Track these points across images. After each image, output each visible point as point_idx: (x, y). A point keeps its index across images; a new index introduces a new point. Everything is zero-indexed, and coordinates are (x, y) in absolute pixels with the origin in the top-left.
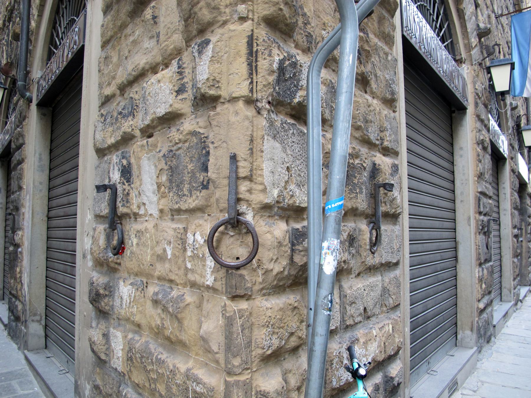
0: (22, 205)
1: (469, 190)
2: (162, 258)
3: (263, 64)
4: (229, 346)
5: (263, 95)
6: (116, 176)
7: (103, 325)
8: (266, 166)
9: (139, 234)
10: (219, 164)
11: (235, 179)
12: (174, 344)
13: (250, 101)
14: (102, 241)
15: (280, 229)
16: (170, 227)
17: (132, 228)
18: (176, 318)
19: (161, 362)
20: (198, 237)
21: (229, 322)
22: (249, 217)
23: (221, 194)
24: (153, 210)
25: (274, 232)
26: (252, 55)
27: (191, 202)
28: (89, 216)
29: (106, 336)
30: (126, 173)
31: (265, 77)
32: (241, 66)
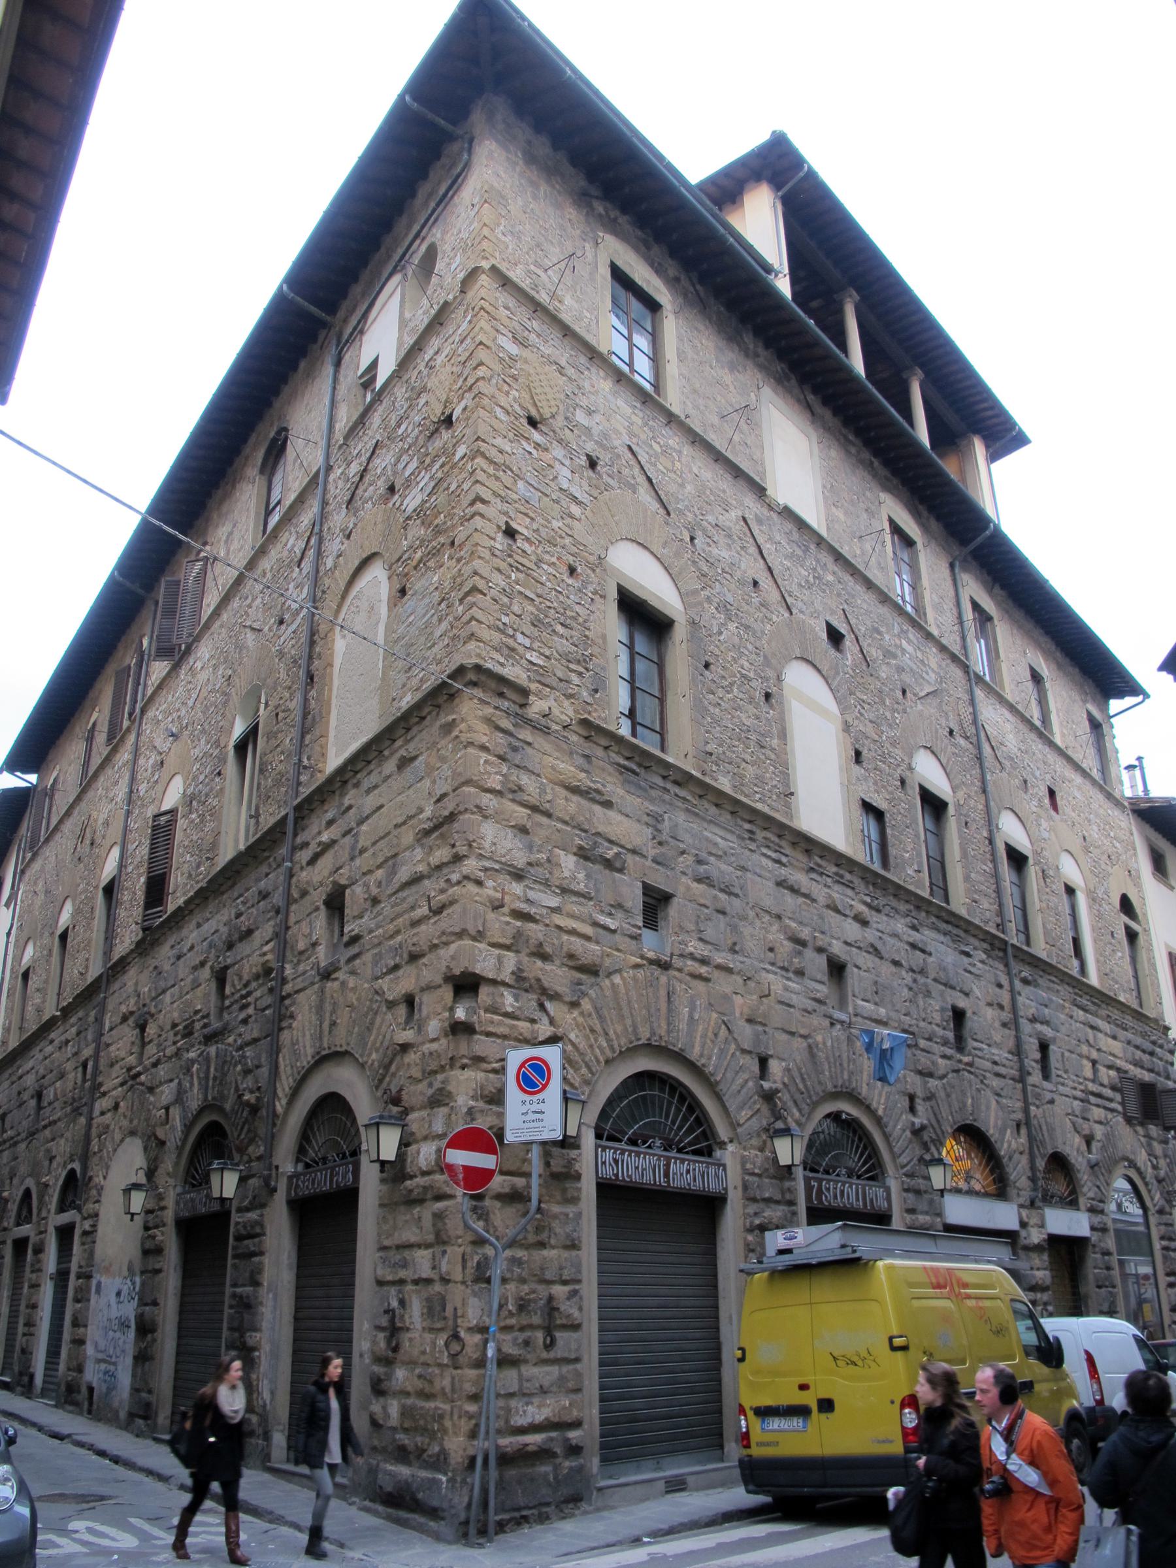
0: (261, 1303)
1: (976, 1262)
2: (424, 1353)
3: (469, 1264)
4: (453, 1390)
5: (469, 1278)
6: (395, 1304)
7: (382, 1399)
8: (470, 1311)
9: (411, 1340)
10: (449, 1312)
11: (456, 1317)
12: (429, 1397)
13: (463, 1283)
14: (383, 1345)
15: (478, 1338)
16: (428, 1336)
17: (405, 1337)
18: (431, 1382)
19: (422, 1408)
20: (441, 1342)
21: (453, 1378)
22: (462, 1334)
23: (451, 1323)
24: (418, 1326)
25: (474, 1339)
26: (464, 1261)
27: (438, 1325)
28: (366, 1326)
29: (384, 1408)
30: (402, 1302)
31: (470, 1271)
32: (459, 1268)
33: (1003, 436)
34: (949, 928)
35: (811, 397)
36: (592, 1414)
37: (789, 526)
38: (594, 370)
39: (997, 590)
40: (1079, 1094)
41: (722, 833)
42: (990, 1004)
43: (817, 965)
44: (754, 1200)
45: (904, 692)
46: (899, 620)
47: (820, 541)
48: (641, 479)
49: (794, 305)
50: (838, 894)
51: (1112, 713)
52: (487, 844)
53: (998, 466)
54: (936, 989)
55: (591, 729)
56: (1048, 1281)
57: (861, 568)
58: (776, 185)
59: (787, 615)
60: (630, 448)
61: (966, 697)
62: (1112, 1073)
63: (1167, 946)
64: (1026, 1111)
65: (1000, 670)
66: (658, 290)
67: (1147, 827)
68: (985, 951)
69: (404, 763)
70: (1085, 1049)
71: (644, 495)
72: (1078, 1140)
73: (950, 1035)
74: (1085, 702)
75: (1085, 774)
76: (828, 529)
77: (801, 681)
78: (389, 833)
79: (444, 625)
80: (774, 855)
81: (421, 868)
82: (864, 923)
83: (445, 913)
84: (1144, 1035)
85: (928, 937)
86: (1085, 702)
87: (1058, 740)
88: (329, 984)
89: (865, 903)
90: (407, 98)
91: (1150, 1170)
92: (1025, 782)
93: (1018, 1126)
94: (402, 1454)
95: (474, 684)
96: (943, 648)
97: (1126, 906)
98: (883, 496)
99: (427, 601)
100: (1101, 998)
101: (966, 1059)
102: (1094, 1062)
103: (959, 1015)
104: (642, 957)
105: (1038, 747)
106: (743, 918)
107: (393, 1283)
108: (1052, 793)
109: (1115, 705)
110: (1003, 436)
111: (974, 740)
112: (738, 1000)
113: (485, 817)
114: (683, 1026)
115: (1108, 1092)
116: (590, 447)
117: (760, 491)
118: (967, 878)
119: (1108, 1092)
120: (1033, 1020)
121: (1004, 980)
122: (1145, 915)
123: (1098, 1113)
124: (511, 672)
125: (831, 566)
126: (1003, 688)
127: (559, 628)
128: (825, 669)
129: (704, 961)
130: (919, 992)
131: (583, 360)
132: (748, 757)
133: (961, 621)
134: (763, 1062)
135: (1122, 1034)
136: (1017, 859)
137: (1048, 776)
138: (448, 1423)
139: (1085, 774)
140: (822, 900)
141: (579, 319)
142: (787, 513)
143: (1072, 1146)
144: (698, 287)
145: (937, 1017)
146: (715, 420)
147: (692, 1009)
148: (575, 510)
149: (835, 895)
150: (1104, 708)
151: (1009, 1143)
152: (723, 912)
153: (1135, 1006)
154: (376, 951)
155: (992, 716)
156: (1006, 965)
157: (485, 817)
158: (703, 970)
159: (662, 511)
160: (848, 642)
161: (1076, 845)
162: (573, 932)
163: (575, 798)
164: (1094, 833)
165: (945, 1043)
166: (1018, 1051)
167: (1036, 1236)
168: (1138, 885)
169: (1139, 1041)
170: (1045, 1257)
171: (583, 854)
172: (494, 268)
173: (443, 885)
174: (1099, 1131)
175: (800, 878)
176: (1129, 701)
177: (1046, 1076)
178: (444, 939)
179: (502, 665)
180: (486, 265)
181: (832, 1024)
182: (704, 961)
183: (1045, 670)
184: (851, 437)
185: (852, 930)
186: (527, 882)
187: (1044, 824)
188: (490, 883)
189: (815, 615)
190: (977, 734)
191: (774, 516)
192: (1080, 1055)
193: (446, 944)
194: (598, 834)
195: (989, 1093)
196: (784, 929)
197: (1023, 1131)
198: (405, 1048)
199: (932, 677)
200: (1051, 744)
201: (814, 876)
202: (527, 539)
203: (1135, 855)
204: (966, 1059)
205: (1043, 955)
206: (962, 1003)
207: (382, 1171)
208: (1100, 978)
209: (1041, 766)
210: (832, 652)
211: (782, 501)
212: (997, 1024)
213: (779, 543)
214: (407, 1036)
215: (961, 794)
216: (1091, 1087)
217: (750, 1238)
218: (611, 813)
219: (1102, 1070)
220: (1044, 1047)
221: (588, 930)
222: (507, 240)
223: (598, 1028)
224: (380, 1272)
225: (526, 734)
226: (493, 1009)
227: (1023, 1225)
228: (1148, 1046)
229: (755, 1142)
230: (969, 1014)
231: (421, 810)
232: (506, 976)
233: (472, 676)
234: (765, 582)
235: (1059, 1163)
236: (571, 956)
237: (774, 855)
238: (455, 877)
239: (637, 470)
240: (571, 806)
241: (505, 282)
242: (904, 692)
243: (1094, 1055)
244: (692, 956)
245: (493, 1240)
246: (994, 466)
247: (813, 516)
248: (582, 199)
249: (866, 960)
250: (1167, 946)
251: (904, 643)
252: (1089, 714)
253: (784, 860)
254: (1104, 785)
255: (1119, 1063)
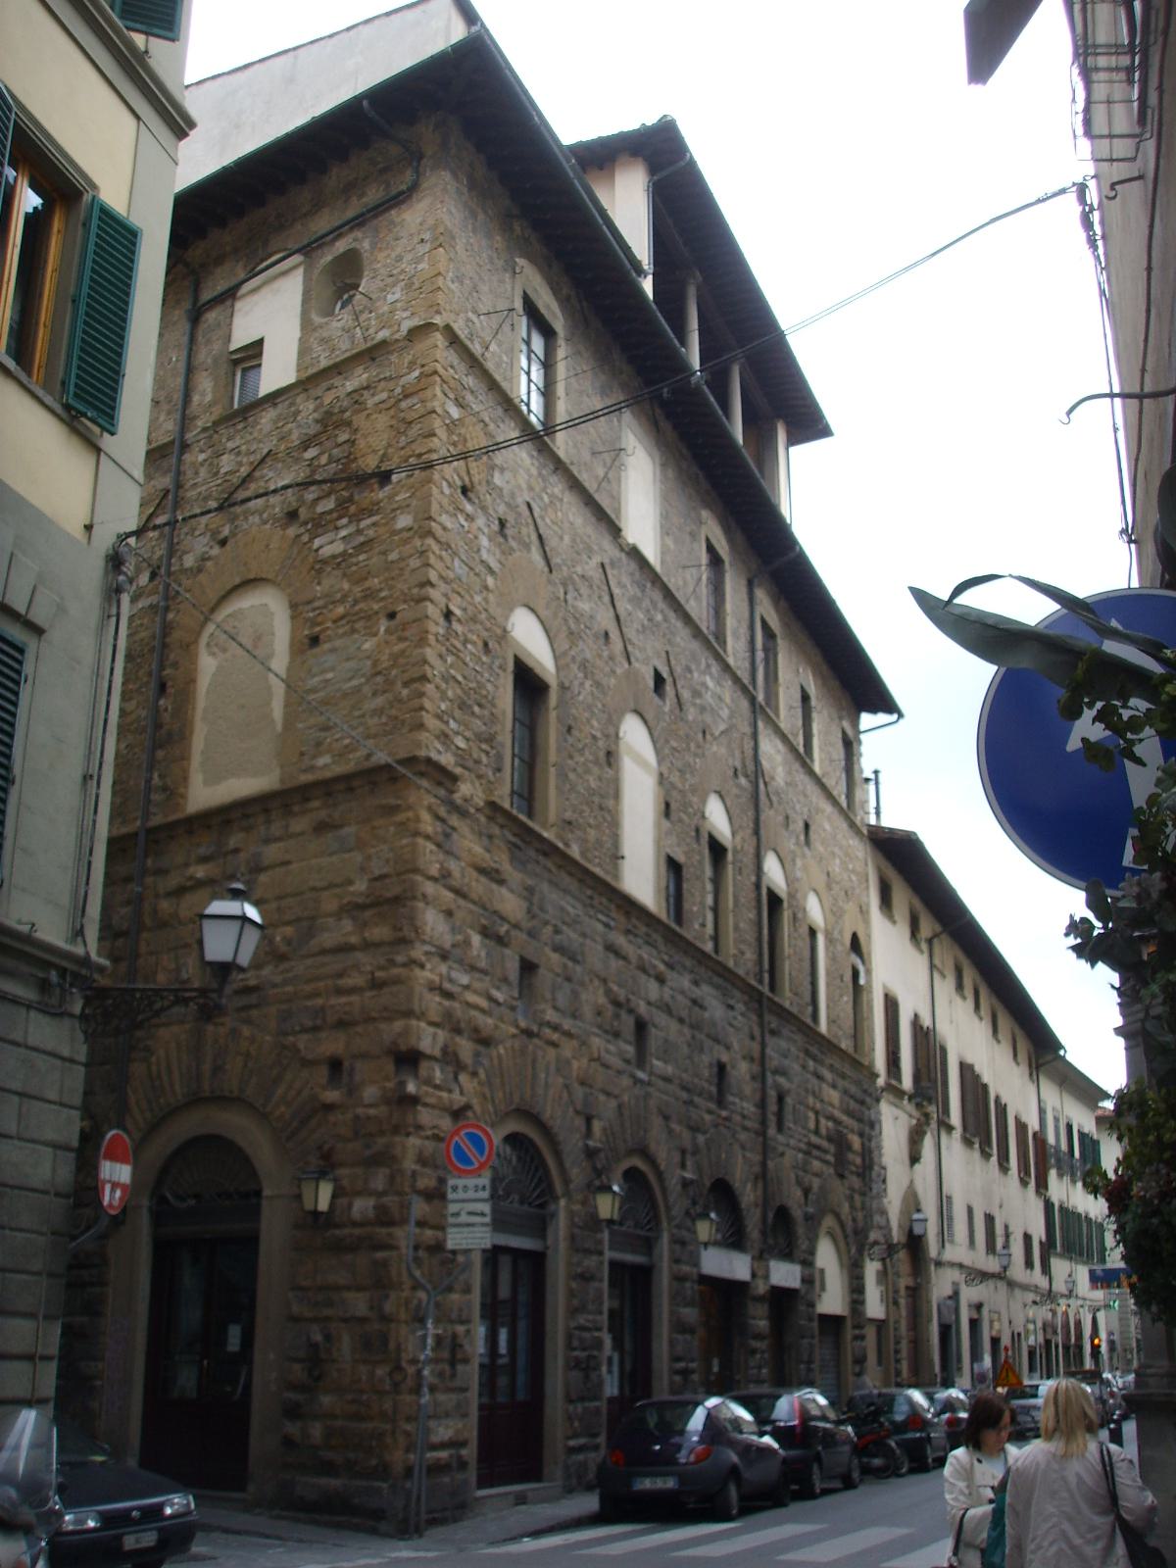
6: (318, 1338)
10: (392, 1345)
22: (404, 1364)
30: (328, 1337)
33: (808, 424)
34: (720, 981)
35: (658, 411)
36: (473, 1435)
37: (633, 566)
38: (507, 420)
39: (783, 603)
40: (803, 1146)
41: (572, 901)
42: (744, 1058)
43: (628, 1024)
44: (577, 1250)
45: (704, 732)
46: (707, 654)
47: (655, 579)
48: (534, 537)
49: (654, 307)
50: (646, 953)
51: (862, 727)
52: (428, 929)
53: (799, 452)
54: (708, 1043)
55: (493, 806)
56: (767, 1331)
57: (683, 602)
58: (653, 169)
59: (626, 666)
60: (529, 505)
61: (748, 730)
62: (830, 1124)
63: (885, 987)
64: (764, 1164)
65: (777, 695)
66: (554, 314)
67: (880, 855)
68: (745, 1004)
69: (321, 828)
70: (811, 1100)
71: (536, 556)
72: (799, 1193)
73: (714, 1089)
74: (841, 718)
75: (835, 802)
76: (663, 562)
77: (634, 734)
78: (301, 893)
79: (380, 701)
80: (604, 918)
81: (354, 940)
82: (661, 980)
83: (386, 990)
84: (858, 1083)
85: (706, 992)
86: (841, 718)
87: (817, 768)
88: (210, 1028)
89: (664, 961)
90: (365, 103)
91: (850, 1223)
92: (787, 817)
93: (756, 1178)
94: (329, 1468)
95: (422, 774)
96: (737, 680)
97: (856, 945)
98: (705, 514)
99: (352, 664)
100: (828, 1045)
101: (724, 1113)
102: (817, 1113)
103: (721, 1068)
104: (517, 1027)
105: (801, 777)
106: (582, 984)
107: (315, 1320)
108: (807, 826)
109: (867, 720)
110: (808, 424)
111: (753, 779)
112: (575, 1064)
113: (427, 904)
114: (540, 1091)
115: (825, 1144)
116: (502, 509)
117: (615, 531)
118: (736, 928)
119: (825, 1144)
120: (776, 1072)
121: (757, 1032)
122: (869, 954)
123: (816, 1164)
124: (447, 759)
125: (661, 605)
126: (778, 715)
127: (476, 709)
128: (649, 717)
129: (556, 1028)
130: (696, 1047)
131: (500, 411)
132: (591, 821)
133: (753, 651)
134: (589, 1120)
135: (841, 1083)
136: (775, 901)
137: (806, 810)
138: (389, 1440)
139: (835, 802)
140: (634, 960)
141: (498, 365)
142: (635, 553)
143: (793, 1198)
144: (585, 304)
145: (706, 1073)
146: (586, 456)
147: (547, 1075)
148: (490, 581)
149: (646, 956)
150: (855, 723)
151: (748, 1195)
152: (569, 979)
153: (851, 1050)
154: (284, 1007)
155: (771, 750)
156: (761, 1016)
157: (427, 904)
158: (555, 1037)
159: (546, 569)
160: (669, 688)
161: (820, 881)
162: (476, 1007)
163: (483, 879)
164: (836, 867)
165: (710, 1098)
166: (762, 1105)
167: (761, 1288)
168: (867, 921)
169: (853, 1089)
170: (766, 1307)
171: (485, 932)
172: (448, 329)
173: (382, 961)
174: (816, 1183)
175: (621, 941)
176: (882, 718)
177: (780, 1127)
178: (385, 1014)
179: (439, 752)
180: (437, 320)
181: (635, 1084)
182: (556, 1028)
183: (812, 691)
184: (685, 451)
185: (653, 989)
186: (450, 963)
187: (799, 863)
188: (428, 966)
189: (646, 661)
190: (756, 773)
191: (623, 555)
192: (808, 1107)
193: (390, 1019)
194: (495, 912)
195: (736, 1147)
196: (608, 992)
197: (760, 1185)
198: (329, 1107)
199: (725, 713)
200: (811, 772)
201: (631, 937)
202: (459, 621)
203: (867, 888)
204: (724, 1113)
205: (787, 1004)
206: (725, 1058)
207: (950, 1298)
208: (829, 1030)
209: (802, 798)
210: (656, 699)
211: (631, 540)
212: (748, 1077)
213: (624, 580)
214: (332, 1096)
215: (738, 838)
216: (814, 1139)
217: (574, 1285)
218: (504, 891)
219: (823, 1121)
220: (781, 1099)
221: (484, 1003)
222: (453, 286)
223: (488, 1095)
224: (296, 1309)
225: (454, 820)
226: (429, 1082)
227: (754, 1275)
228: (860, 1095)
229: (580, 1197)
230: (729, 1068)
231: (350, 882)
232: (437, 1052)
233: (423, 768)
234: (614, 635)
235: (783, 1214)
236: (476, 1030)
237: (604, 918)
238: (400, 959)
239: (532, 527)
240: (479, 886)
241: (453, 340)
242: (704, 732)
243: (818, 1106)
244: (548, 1024)
245: (429, 1286)
246: (792, 449)
247: (651, 553)
248: (505, 222)
249: (661, 1019)
250: (885, 987)
251: (708, 678)
252: (844, 733)
253: (612, 923)
254: (848, 811)
255: (837, 1113)
